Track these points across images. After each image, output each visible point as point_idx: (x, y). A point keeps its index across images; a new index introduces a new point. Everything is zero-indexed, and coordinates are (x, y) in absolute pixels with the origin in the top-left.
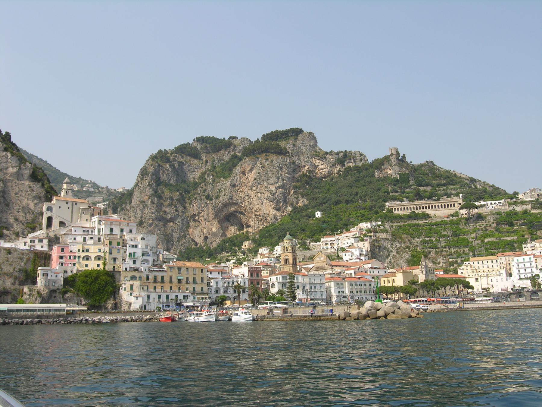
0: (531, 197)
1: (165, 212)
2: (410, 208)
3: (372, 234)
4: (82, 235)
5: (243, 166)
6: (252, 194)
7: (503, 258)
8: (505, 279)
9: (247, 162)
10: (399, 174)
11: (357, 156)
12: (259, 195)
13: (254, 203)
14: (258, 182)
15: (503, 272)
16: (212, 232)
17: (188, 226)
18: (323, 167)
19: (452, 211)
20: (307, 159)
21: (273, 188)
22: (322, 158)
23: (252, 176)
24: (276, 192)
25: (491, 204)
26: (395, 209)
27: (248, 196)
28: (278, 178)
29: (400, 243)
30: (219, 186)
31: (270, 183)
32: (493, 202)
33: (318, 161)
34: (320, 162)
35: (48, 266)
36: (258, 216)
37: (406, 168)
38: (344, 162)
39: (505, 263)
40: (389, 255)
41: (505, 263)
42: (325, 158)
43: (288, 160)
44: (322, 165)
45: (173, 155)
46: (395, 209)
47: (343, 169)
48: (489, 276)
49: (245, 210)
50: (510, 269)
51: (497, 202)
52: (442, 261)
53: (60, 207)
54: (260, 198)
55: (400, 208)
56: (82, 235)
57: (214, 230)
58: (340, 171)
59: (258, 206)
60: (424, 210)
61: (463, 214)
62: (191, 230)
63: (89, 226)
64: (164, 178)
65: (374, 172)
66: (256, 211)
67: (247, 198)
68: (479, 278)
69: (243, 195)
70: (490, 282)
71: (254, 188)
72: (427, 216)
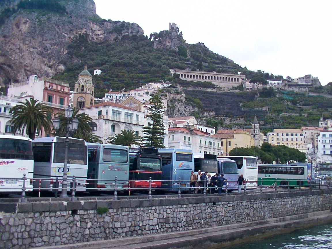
0: (306, 82)
4: (326, 149)
5: (16, 19)
6: (24, 48)
9: (22, 14)
12: (32, 50)
13: (25, 57)
14: (32, 33)
18: (99, 33)
19: (236, 84)
22: (100, 24)
23: (24, 28)
26: (182, 75)
27: (19, 49)
33: (96, 26)
34: (98, 27)
35: (63, 104)
36: (28, 71)
38: (121, 31)
42: (103, 24)
44: (99, 30)
46: (182, 75)
47: (120, 37)
49: (14, 64)
54: (31, 53)
55: (189, 76)
56: (326, 149)
58: (117, 38)
59: (29, 61)
60: (210, 81)
61: (248, 89)
63: (128, 122)
66: (25, 66)
67: (17, 51)
69: (12, 46)
71: (27, 42)
72: (213, 87)
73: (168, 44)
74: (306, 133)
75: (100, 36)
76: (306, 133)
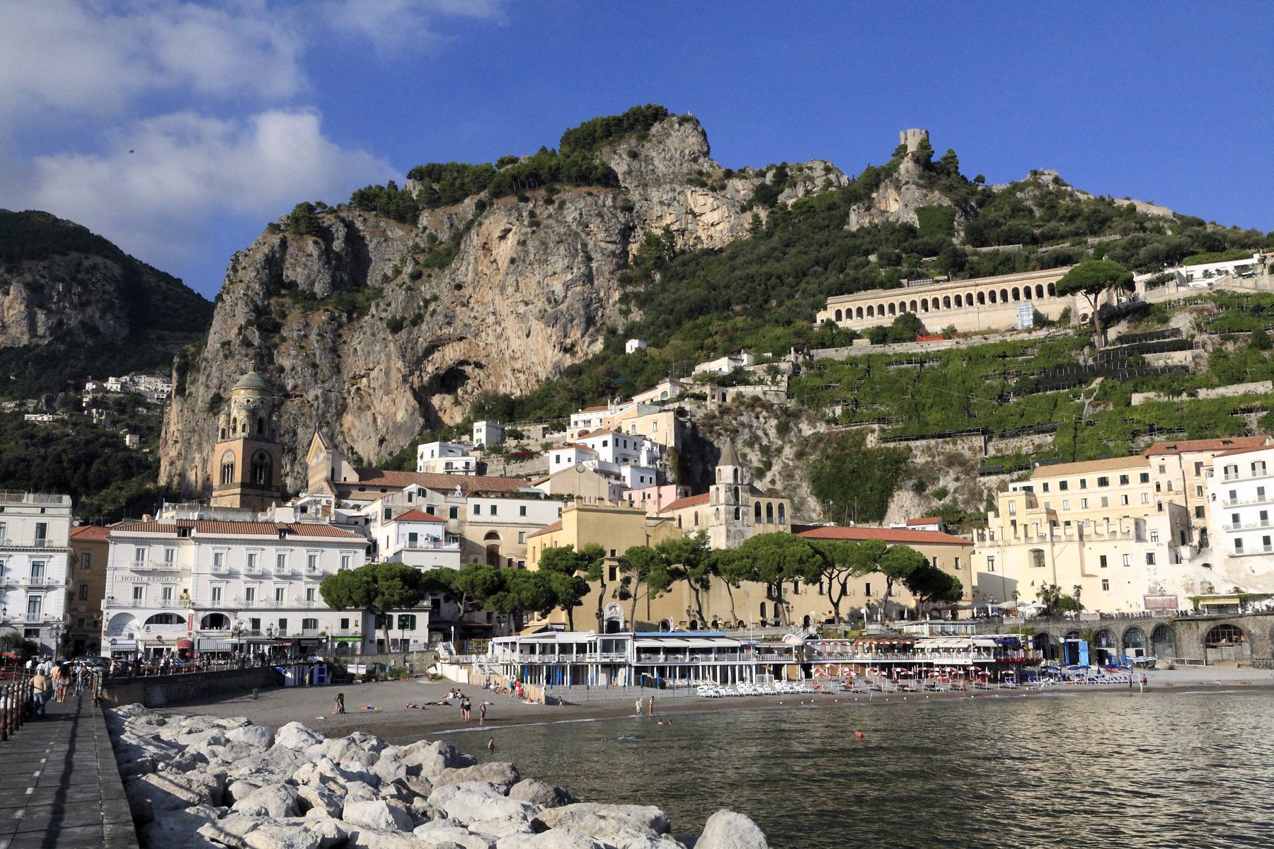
1: (282, 370)
2: (903, 305)
3: (707, 390)
7: (1171, 460)
8: (1162, 555)
10: (919, 211)
11: (815, 174)
12: (522, 309)
15: (1161, 525)
16: (395, 423)
17: (342, 410)
18: (715, 217)
20: (671, 194)
21: (558, 287)
24: (566, 297)
25: (1207, 274)
27: (494, 313)
28: (575, 255)
29: (812, 423)
30: (426, 289)
31: (550, 270)
32: (1212, 267)
33: (701, 200)
37: (948, 190)
39: (1178, 486)
40: (769, 466)
41: (1178, 486)
43: (609, 202)
45: (663, 316)
48: (1079, 536)
50: (1200, 512)
51: (1230, 266)
52: (952, 486)
53: (1106, 587)
57: (401, 416)
62: (348, 419)
64: (295, 273)
65: (847, 215)
67: (491, 319)
68: (1046, 548)
70: (1093, 565)
71: (510, 290)
73: (894, 207)
74: (1162, 469)
75: (718, 228)
76: (1162, 469)
